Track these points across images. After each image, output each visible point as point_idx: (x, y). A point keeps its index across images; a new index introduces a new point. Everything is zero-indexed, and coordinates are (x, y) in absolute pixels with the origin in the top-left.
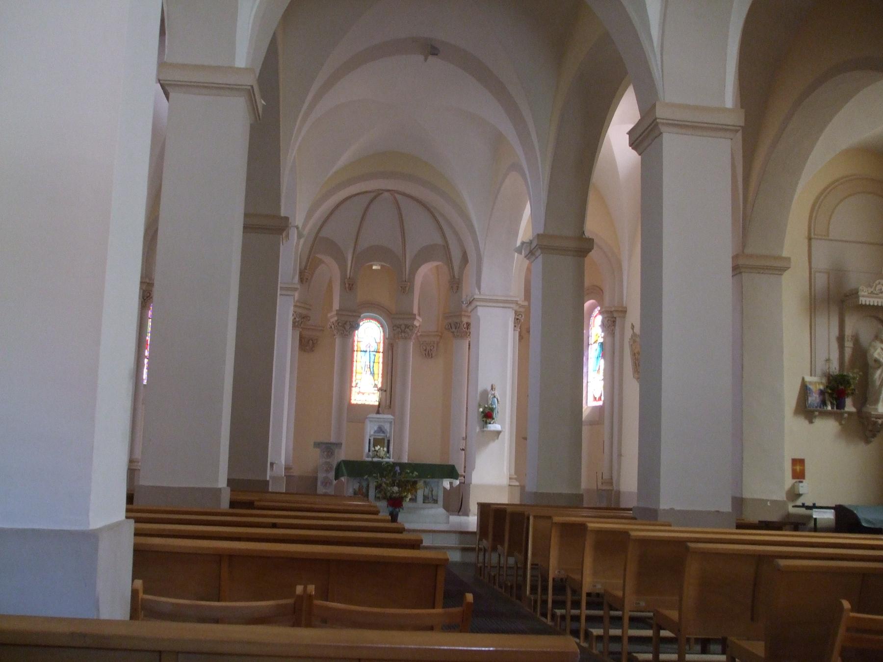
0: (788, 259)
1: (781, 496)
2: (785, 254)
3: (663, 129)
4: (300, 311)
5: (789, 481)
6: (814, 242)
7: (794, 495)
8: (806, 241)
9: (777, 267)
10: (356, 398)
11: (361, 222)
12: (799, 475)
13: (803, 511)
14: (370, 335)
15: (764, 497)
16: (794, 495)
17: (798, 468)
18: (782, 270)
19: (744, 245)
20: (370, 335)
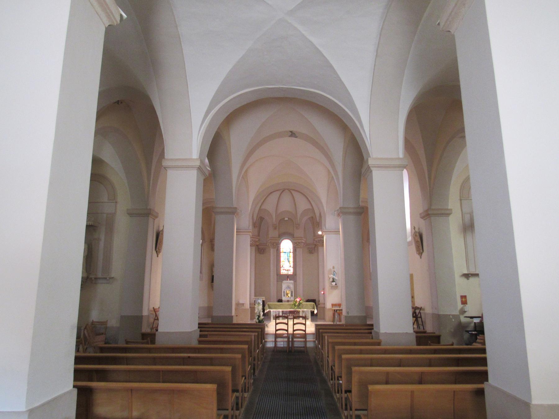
0: (451, 210)
1: (456, 313)
2: (449, 208)
3: (372, 169)
4: (254, 239)
5: (460, 306)
6: (463, 201)
7: (463, 312)
8: (459, 201)
9: (447, 213)
10: (283, 272)
11: (278, 201)
12: (464, 302)
13: (469, 320)
14: (286, 246)
15: (449, 314)
16: (463, 312)
17: (464, 300)
18: (448, 215)
19: (430, 204)
20: (286, 246)
